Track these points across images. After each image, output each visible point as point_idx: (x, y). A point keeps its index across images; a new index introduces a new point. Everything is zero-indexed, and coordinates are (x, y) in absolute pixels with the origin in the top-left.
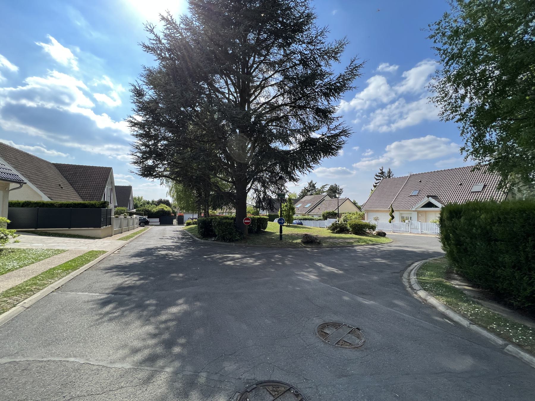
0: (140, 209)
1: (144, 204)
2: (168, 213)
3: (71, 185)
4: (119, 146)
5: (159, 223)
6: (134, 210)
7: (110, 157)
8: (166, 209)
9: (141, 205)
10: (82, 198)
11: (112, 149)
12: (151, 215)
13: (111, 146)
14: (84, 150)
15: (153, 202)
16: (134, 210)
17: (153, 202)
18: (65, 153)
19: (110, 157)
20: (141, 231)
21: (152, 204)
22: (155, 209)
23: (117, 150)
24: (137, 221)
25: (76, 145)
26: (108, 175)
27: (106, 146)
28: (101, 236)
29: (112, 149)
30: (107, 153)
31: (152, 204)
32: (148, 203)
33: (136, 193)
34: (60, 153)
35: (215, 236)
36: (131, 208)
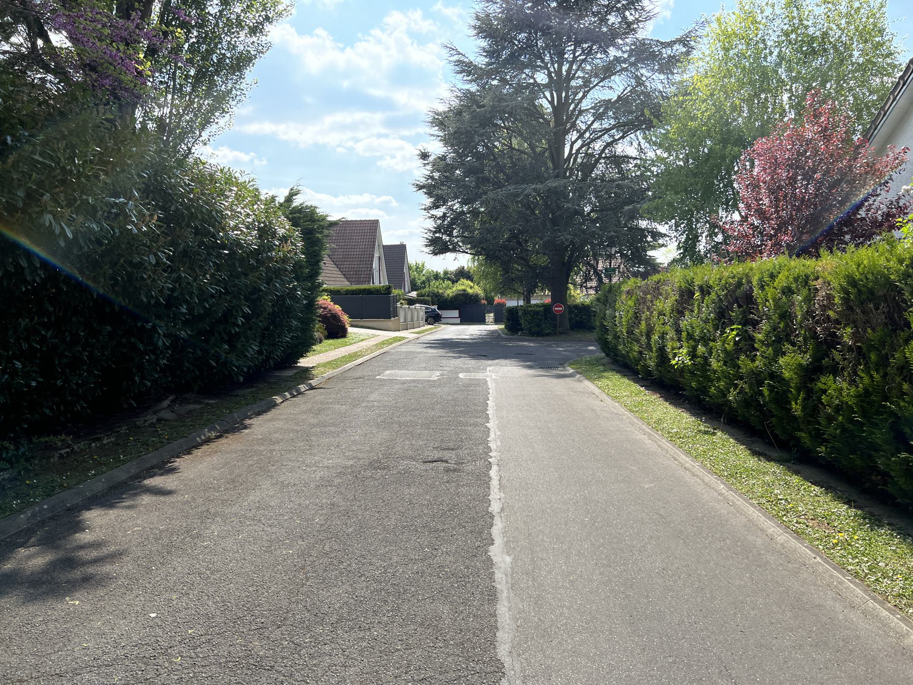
0: (423, 291)
1: (428, 279)
2: (474, 299)
3: (340, 269)
4: (358, 116)
5: (458, 321)
6: (414, 294)
7: (340, 150)
8: (470, 291)
9: (423, 282)
10: (351, 282)
11: (344, 127)
12: (446, 304)
13: (340, 117)
14: (285, 137)
15: (446, 273)
16: (414, 294)
17: (446, 273)
18: (247, 153)
19: (340, 150)
20: (431, 329)
21: (443, 279)
22: (451, 291)
23: (354, 127)
24: (422, 314)
25: (267, 127)
26: (374, 242)
27: (329, 120)
28: (393, 327)
29: (344, 127)
30: (332, 139)
31: (443, 279)
32: (436, 277)
33: (491, 548)
34: (236, 153)
35: (522, 330)
36: (407, 290)
